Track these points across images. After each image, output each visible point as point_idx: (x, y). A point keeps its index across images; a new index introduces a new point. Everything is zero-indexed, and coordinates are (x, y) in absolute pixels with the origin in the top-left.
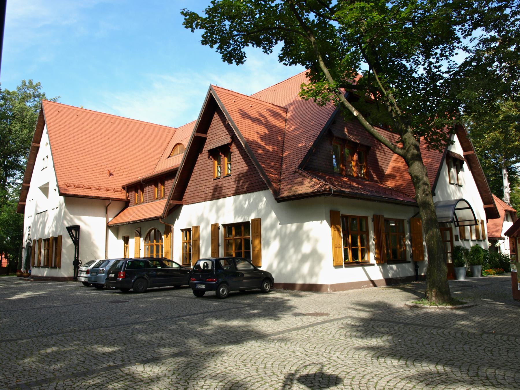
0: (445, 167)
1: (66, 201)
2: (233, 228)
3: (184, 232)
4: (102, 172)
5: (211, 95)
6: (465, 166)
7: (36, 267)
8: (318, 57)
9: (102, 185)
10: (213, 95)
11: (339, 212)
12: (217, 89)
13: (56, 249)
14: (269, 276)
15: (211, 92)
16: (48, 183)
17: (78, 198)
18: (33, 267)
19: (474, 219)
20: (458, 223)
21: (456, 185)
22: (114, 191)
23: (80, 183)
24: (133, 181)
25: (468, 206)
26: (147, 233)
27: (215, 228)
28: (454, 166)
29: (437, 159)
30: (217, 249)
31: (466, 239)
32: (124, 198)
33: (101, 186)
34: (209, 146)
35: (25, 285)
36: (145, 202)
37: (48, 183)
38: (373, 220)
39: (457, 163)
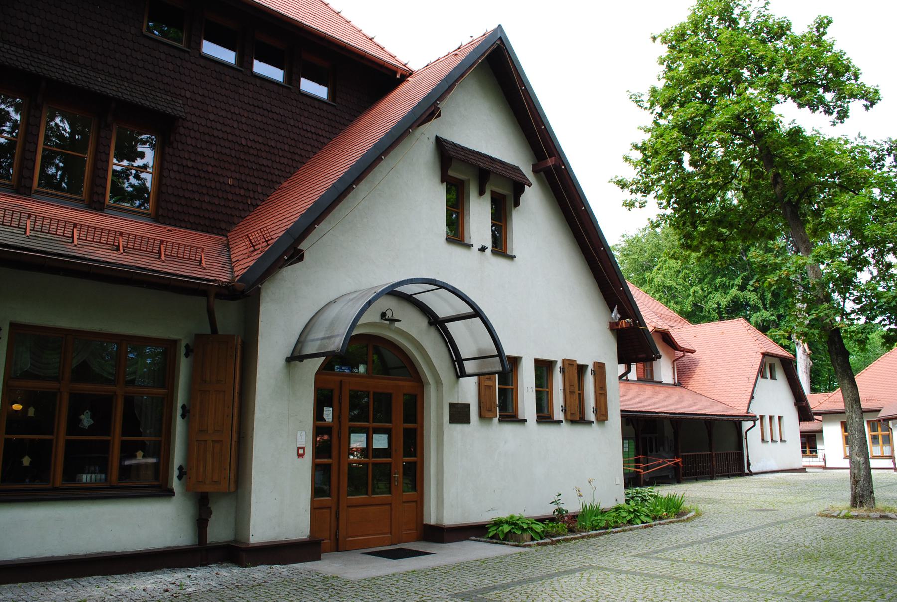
21: (483, 249)
25: (468, 310)
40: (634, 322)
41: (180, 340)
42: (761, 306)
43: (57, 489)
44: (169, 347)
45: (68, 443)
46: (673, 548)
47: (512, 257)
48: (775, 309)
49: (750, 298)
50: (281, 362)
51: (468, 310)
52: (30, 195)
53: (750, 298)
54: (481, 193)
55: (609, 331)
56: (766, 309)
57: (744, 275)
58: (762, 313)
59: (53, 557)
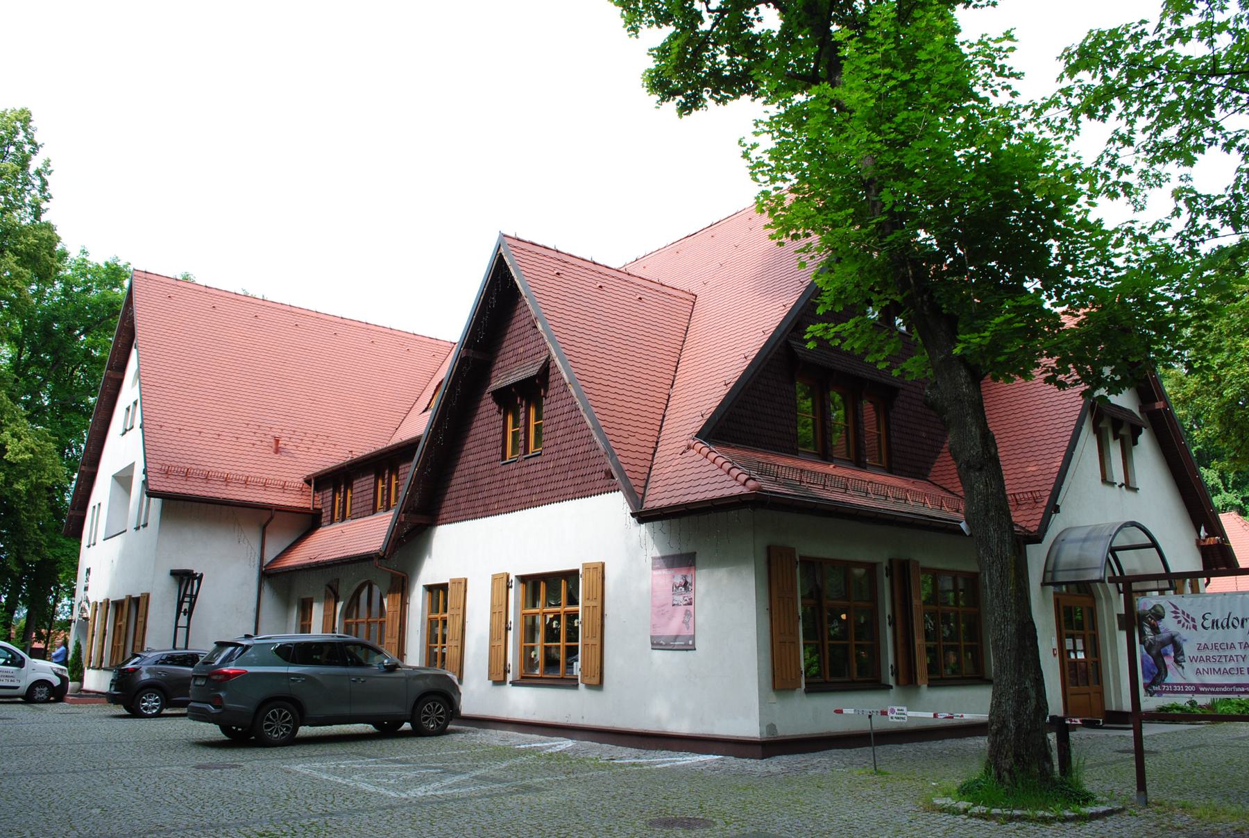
0: (1088, 445)
1: (166, 513)
3: (530, 583)
4: (259, 443)
6: (1144, 439)
7: (93, 668)
9: (255, 473)
11: (793, 551)
12: (515, 243)
14: (456, 698)
16: (134, 463)
18: (89, 668)
21: (1120, 486)
23: (202, 468)
24: (332, 465)
25: (1148, 541)
26: (351, 592)
27: (502, 583)
28: (1115, 438)
29: (1067, 419)
30: (503, 638)
32: (307, 506)
33: (252, 474)
36: (354, 516)
37: (134, 463)
38: (890, 572)
39: (1122, 432)
40: (1221, 539)
41: (882, 563)
42: (1221, 487)
43: (853, 682)
44: (871, 568)
45: (577, 640)
46: (1177, 750)
47: (1135, 490)
48: (1238, 490)
49: (1207, 477)
50: (1040, 586)
51: (1148, 541)
52: (865, 468)
53: (1207, 477)
54: (1115, 438)
55: (1196, 547)
56: (1226, 490)
57: (1198, 449)
58: (1223, 496)
59: (830, 733)
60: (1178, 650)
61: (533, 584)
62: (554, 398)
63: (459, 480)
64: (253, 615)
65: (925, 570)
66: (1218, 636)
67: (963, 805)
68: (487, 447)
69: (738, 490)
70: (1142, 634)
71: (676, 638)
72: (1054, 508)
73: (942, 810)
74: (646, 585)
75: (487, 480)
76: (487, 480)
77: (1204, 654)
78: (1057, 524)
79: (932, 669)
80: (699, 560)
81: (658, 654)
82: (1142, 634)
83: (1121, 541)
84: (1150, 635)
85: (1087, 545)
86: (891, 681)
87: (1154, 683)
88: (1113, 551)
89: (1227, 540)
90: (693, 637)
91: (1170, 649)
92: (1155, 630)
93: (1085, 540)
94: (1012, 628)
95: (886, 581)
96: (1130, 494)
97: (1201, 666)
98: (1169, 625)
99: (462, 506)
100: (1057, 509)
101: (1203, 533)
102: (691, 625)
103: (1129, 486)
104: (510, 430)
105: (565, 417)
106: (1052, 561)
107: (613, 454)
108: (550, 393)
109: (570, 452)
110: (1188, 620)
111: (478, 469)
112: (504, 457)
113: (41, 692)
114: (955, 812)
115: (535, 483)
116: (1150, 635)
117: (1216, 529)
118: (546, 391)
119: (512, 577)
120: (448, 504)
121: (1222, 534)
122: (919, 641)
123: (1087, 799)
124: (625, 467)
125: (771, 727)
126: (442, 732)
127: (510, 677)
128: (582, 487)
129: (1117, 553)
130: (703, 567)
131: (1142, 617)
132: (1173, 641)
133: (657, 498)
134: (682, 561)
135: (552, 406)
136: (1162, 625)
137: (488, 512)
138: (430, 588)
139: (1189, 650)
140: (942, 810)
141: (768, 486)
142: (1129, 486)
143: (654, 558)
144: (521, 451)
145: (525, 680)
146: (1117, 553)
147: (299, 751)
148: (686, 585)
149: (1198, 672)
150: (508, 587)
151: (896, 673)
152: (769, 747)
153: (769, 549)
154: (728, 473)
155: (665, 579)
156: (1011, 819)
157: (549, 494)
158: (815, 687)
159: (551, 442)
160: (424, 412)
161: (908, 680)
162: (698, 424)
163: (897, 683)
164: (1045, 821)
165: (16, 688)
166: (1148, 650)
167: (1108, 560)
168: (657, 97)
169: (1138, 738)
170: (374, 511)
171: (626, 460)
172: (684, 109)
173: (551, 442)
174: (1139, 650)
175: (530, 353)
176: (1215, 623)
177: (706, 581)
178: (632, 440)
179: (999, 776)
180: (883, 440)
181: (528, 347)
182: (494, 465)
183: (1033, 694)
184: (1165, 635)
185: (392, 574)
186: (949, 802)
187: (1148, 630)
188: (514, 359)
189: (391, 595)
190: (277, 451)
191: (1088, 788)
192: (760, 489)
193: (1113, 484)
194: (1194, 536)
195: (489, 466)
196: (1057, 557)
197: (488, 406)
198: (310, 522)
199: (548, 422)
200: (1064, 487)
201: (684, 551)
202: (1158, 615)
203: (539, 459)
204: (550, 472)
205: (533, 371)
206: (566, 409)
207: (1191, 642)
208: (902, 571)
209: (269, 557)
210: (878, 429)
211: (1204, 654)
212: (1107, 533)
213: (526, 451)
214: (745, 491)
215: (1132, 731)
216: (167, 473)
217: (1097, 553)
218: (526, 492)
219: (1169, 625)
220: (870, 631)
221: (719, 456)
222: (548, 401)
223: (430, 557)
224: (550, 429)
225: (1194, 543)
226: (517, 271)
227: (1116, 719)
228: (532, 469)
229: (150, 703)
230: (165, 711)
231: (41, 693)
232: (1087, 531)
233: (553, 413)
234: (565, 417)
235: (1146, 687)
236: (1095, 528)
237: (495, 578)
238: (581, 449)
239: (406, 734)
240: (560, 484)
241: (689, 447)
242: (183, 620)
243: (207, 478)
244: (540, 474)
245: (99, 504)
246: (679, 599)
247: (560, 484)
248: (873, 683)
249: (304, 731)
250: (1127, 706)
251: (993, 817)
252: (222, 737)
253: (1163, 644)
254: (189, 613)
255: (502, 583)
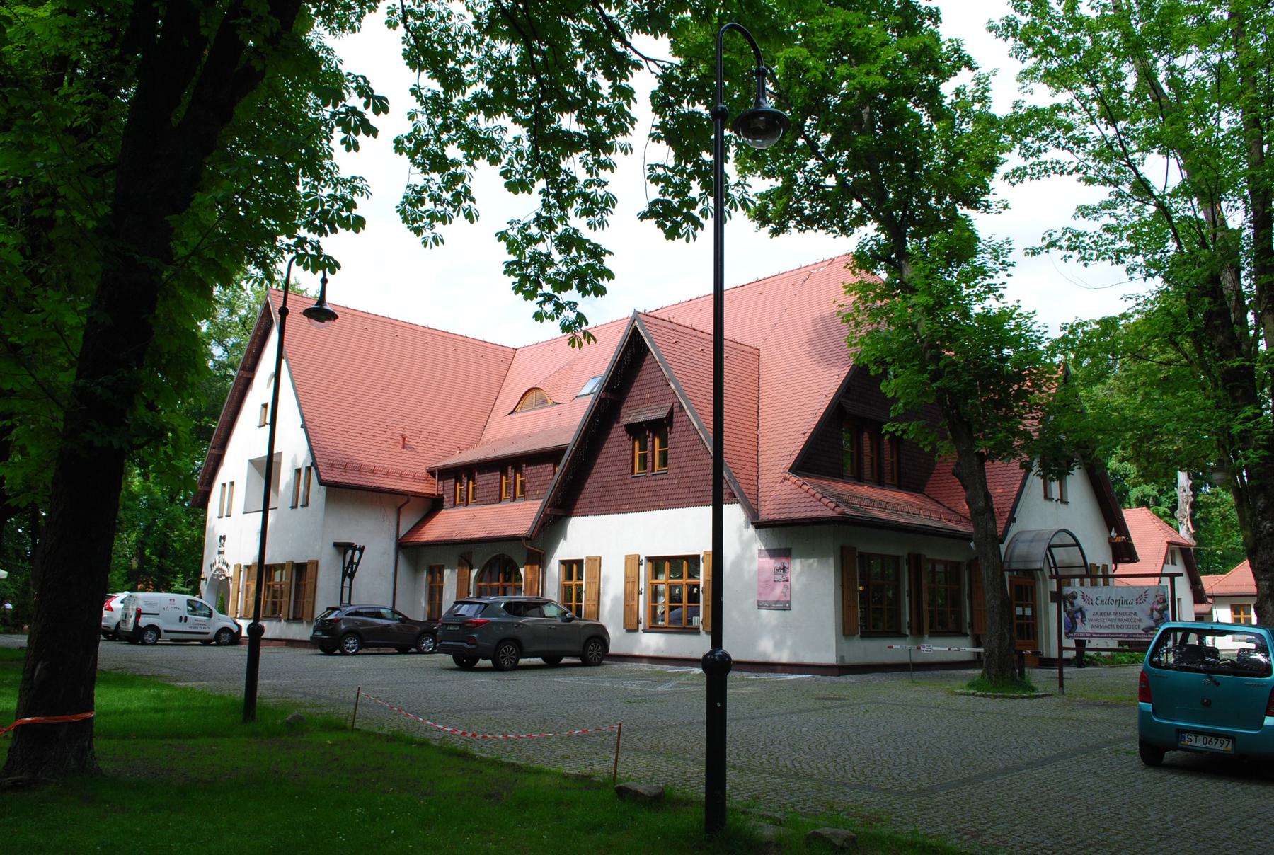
2: (667, 564)
5: (635, 330)
8: (860, 220)
10: (640, 330)
13: (296, 602)
15: (637, 323)
17: (395, 527)
19: (1083, 563)
20: (1056, 572)
22: (414, 478)
27: (633, 562)
31: (612, 650)
34: (630, 416)
35: (968, 620)
38: (909, 563)
47: (1067, 503)
60: (1083, 615)
61: (657, 563)
62: (678, 434)
63: (591, 485)
64: (391, 578)
65: (929, 560)
66: (1104, 608)
67: (972, 691)
68: (618, 463)
69: (829, 513)
70: (1065, 606)
71: (777, 602)
72: (1012, 520)
73: (962, 694)
74: (755, 566)
75: (619, 487)
76: (619, 487)
77: (1096, 618)
78: (1014, 529)
79: (931, 626)
80: (793, 552)
81: (764, 612)
82: (1065, 606)
83: (1056, 541)
84: (1069, 607)
85: (1033, 544)
86: (908, 632)
87: (1070, 632)
88: (1050, 548)
89: (1130, 540)
90: (789, 602)
91: (1079, 614)
92: (1072, 604)
93: (1032, 541)
94: (998, 602)
95: (906, 568)
96: (1063, 506)
97: (1094, 624)
98: (1079, 602)
99: (596, 504)
100: (1014, 520)
101: (1114, 534)
102: (788, 594)
103: (1063, 500)
104: (637, 453)
105: (687, 449)
106: (1010, 551)
107: (735, 482)
108: (674, 430)
109: (692, 474)
110: (1089, 600)
111: (610, 479)
112: (633, 473)
113: (225, 637)
114: (969, 695)
115: (662, 493)
116: (1069, 607)
117: (1121, 528)
118: (671, 428)
119: (642, 558)
120: (582, 501)
121: (1127, 534)
122: (925, 607)
123: (1034, 689)
124: (744, 491)
125: (842, 658)
126: (599, 664)
127: (641, 627)
128: (703, 499)
129: (1053, 549)
130: (797, 557)
131: (1065, 598)
132: (1081, 611)
133: (768, 511)
134: (781, 553)
135: (676, 440)
136: (1076, 602)
137: (619, 510)
138: (563, 562)
139: (1088, 615)
140: (962, 694)
141: (849, 511)
142: (1063, 500)
143: (760, 550)
144: (649, 469)
145: (652, 629)
146: (1053, 549)
147: (561, 671)
148: (784, 569)
149: (1092, 626)
150: (640, 564)
151: (911, 627)
152: (841, 669)
153: (842, 548)
154: (820, 500)
155: (770, 563)
156: (996, 697)
157: (673, 502)
158: (865, 635)
159: (676, 466)
160: (512, 412)
161: (918, 632)
162: (789, 462)
163: (911, 633)
164: (1014, 698)
165: (207, 633)
166: (1068, 615)
167: (1046, 555)
168: (756, 224)
169: (1061, 673)
170: (500, 501)
171: (745, 486)
172: (775, 233)
173: (676, 466)
174: (1063, 614)
175: (656, 399)
176: (1102, 602)
177: (796, 566)
178: (744, 471)
179: (990, 678)
180: (895, 466)
181: (654, 394)
182: (624, 477)
183: (1008, 636)
184: (1077, 607)
185: (529, 550)
186: (963, 691)
187: (1068, 604)
188: (641, 402)
189: (529, 567)
190: (404, 447)
191: (1034, 685)
192: (844, 513)
193: (1051, 499)
194: (1107, 536)
195: (620, 478)
196: (1012, 552)
197: (618, 434)
198: (433, 506)
199: (672, 451)
200: (1021, 502)
201: (783, 546)
202: (1074, 596)
203: (665, 476)
204: (674, 487)
205: (662, 414)
206: (688, 443)
207: (1090, 611)
208: (916, 561)
209: (403, 532)
210: (892, 457)
211: (1096, 618)
212: (1046, 537)
213: (653, 470)
214: (835, 514)
215: (1057, 657)
216: (331, 466)
217: (1040, 550)
218: (654, 499)
219: (1079, 602)
220: (897, 600)
221: (809, 485)
222: (673, 436)
223: (565, 539)
224: (675, 456)
225: (1107, 540)
226: (651, 342)
227: (1047, 663)
228: (659, 483)
229: (351, 644)
230: (360, 651)
231: (225, 637)
232: (1033, 534)
233: (676, 445)
234: (687, 449)
235: (1066, 634)
236: (1038, 532)
237: (628, 558)
238: (701, 473)
239: (1034, 611)
240: (684, 496)
241: (786, 479)
242: (347, 580)
243: (360, 470)
244: (666, 487)
245: (232, 483)
246: (779, 577)
247: (684, 496)
248: (896, 633)
249: (522, 661)
250: (1054, 654)
251: (988, 696)
252: (455, 666)
253: (1076, 612)
254: (352, 576)
255: (633, 562)
